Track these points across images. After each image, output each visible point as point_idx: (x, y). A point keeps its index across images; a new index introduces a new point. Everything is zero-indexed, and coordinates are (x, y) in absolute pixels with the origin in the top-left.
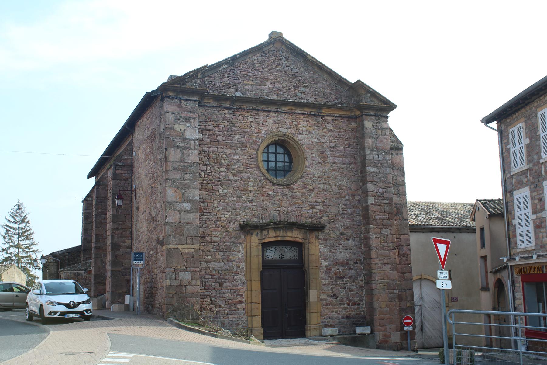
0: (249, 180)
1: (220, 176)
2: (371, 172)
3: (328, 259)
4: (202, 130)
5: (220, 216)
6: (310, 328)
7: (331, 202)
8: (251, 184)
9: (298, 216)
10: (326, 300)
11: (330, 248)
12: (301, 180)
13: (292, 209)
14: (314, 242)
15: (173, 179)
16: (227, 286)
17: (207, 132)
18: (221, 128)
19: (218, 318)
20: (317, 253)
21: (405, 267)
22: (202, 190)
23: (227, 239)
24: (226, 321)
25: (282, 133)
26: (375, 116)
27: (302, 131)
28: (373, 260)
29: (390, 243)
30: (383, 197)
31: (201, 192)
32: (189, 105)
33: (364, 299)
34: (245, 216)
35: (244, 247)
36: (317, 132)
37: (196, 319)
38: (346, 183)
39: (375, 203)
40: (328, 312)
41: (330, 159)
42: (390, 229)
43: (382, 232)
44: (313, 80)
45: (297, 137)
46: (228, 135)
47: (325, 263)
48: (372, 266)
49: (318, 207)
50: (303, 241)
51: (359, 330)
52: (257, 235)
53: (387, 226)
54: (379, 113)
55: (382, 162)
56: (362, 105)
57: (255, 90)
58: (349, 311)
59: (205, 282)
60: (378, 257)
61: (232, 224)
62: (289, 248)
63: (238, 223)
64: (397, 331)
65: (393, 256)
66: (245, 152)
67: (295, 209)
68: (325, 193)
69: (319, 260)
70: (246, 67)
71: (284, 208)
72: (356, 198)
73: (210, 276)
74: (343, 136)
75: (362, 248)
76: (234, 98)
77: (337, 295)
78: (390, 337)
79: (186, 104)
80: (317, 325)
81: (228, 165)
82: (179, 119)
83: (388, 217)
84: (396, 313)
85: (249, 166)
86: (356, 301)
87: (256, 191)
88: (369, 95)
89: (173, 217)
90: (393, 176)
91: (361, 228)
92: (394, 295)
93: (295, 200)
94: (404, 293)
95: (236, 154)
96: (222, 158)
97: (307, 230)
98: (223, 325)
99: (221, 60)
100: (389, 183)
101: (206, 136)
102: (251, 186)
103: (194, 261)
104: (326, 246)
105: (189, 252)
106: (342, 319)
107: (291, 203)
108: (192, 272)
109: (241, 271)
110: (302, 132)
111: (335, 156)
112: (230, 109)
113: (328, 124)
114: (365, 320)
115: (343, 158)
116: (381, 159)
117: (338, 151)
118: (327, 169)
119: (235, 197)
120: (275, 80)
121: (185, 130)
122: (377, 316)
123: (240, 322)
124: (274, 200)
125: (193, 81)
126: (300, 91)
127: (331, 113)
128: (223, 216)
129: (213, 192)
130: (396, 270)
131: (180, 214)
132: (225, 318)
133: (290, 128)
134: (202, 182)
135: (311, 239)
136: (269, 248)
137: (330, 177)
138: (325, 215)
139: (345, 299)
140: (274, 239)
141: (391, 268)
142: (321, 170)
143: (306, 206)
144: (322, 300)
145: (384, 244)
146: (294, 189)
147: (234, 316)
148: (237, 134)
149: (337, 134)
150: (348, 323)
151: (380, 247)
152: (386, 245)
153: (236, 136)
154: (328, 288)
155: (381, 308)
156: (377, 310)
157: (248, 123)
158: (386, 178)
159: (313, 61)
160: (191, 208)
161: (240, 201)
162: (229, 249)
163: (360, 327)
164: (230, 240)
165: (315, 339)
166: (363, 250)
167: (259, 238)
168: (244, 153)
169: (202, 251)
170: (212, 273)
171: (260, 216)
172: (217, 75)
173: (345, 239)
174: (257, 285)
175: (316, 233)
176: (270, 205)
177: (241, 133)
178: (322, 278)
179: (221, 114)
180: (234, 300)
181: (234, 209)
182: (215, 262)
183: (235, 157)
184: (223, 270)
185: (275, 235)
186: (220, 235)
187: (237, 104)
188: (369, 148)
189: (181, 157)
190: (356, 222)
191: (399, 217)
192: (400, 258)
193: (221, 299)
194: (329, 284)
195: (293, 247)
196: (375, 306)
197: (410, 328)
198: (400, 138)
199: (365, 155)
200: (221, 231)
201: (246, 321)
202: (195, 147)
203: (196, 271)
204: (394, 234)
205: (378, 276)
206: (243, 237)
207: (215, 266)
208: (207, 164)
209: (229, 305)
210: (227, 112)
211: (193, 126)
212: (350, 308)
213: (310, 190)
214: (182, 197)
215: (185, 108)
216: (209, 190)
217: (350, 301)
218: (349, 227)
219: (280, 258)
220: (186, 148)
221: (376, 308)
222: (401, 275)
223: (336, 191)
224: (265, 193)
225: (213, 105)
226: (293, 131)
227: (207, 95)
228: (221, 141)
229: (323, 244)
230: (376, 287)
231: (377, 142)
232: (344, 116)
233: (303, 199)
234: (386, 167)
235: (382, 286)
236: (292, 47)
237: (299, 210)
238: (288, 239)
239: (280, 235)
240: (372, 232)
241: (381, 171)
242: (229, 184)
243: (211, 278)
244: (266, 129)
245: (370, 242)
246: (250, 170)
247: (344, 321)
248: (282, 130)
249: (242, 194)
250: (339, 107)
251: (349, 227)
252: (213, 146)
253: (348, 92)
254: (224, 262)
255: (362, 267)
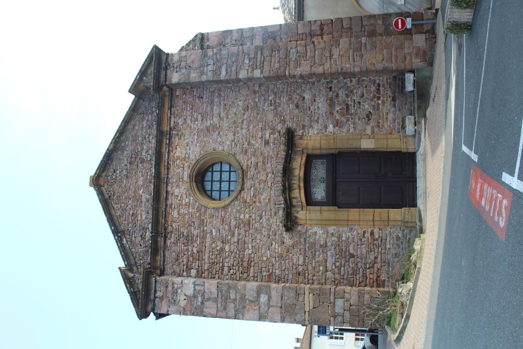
0: (237, 219)
1: (234, 252)
2: (227, 73)
3: (326, 123)
4: (187, 269)
5: (277, 254)
6: (405, 149)
7: (261, 120)
8: (242, 217)
9: (277, 161)
10: (373, 128)
11: (313, 121)
12: (238, 157)
13: (270, 168)
14: (306, 142)
15: (235, 312)
16: (354, 249)
17: (189, 263)
18: (185, 247)
19: (389, 261)
20: (318, 138)
21: (335, 27)
22: (248, 273)
23: (302, 246)
24: (393, 251)
25: (188, 179)
26: (166, 70)
27: (186, 155)
28: (326, 70)
29: (306, 49)
30: (254, 58)
31: (251, 274)
32: (160, 288)
33: (372, 78)
34: (276, 225)
35: (310, 227)
36: (187, 136)
37: (389, 295)
38: (240, 101)
39: (261, 69)
40: (387, 124)
41: (216, 120)
42: (291, 49)
43: (294, 59)
44: (134, 141)
45: (192, 160)
46: (191, 240)
47: (331, 128)
48: (333, 71)
49: (267, 136)
50: (305, 155)
51: (409, 87)
52: (298, 212)
53: (287, 53)
54: (164, 66)
55: (215, 60)
56: (154, 88)
57: (146, 207)
58: (387, 97)
59: (348, 274)
60: (323, 65)
61: (285, 240)
62: (313, 171)
63: (285, 233)
64: (411, 39)
65: (322, 45)
66: (208, 221)
67: (269, 164)
68: (251, 127)
69: (327, 135)
70: (124, 217)
71: (268, 178)
72: (257, 89)
73: (342, 268)
74: (191, 105)
75: (314, 81)
76: (153, 234)
77: (368, 113)
78: (418, 48)
79: (159, 292)
80: (402, 139)
81: (223, 242)
82: (175, 301)
83: (276, 52)
84: (390, 39)
85: (223, 217)
86: (375, 89)
87: (250, 210)
88: (144, 78)
89: (275, 315)
90: (232, 44)
91: (291, 83)
92: (368, 43)
93: (259, 164)
94: (366, 27)
95: (211, 232)
96: (216, 248)
97: (292, 151)
98: (397, 256)
99: (117, 247)
100: (239, 52)
101: (193, 265)
102: (244, 216)
103: (323, 293)
104: (311, 126)
105: (313, 299)
106: (395, 107)
107: (262, 169)
108: (336, 296)
109: (338, 232)
110: (187, 154)
111: (211, 114)
112: (166, 237)
113: (178, 123)
114: (398, 77)
115: (214, 105)
116: (212, 61)
117: (207, 111)
118: (225, 124)
119: (256, 235)
120: (136, 185)
121: (185, 295)
122: (393, 66)
123: (394, 235)
124: (259, 189)
125: (136, 282)
126: (146, 156)
127: (168, 119)
128: (276, 251)
129: (251, 260)
130: (338, 41)
131: (272, 306)
132: (389, 253)
133: (184, 169)
134: (240, 273)
135: (303, 145)
136: (312, 195)
137: (235, 121)
138: (276, 127)
139: (373, 103)
140: (302, 191)
141: (336, 47)
142: (227, 131)
143: (267, 150)
144: (373, 132)
145: (307, 57)
146: (247, 165)
147: (387, 242)
148: (191, 230)
149: (188, 112)
150: (401, 99)
151: (311, 62)
152: (309, 53)
153: (193, 231)
154: (359, 125)
155: (383, 59)
156: (386, 65)
157: (179, 217)
158: (233, 54)
159: (115, 142)
160: (265, 294)
161: (261, 230)
162: (313, 244)
163: (406, 86)
164: (303, 243)
165: (418, 145)
166: (315, 80)
167: (301, 209)
168: (210, 223)
169: (314, 276)
170: (339, 266)
171: (277, 206)
172: (133, 250)
173: (303, 103)
174: (354, 213)
175: (296, 138)
176: (265, 195)
177: (189, 226)
178: (347, 132)
179: (171, 247)
180: (370, 241)
181: (269, 238)
182: (327, 262)
183: (214, 234)
184: (336, 253)
185: (298, 190)
186: (297, 255)
187: (160, 230)
188: (200, 77)
189: (213, 301)
190: (283, 89)
191: (278, 35)
192: (325, 34)
193: (368, 257)
194: (354, 123)
195: (312, 166)
196: (381, 68)
197: (409, 21)
198: (191, 38)
199: (209, 81)
200: (292, 253)
201: (394, 227)
202: (202, 285)
203: (334, 293)
204: (297, 43)
205: (346, 64)
206: (299, 228)
207: (331, 262)
208: (222, 265)
209: (375, 248)
210: (169, 240)
211: (181, 285)
212: (383, 96)
213: (248, 146)
214: (253, 303)
215: (163, 293)
216: (249, 265)
217: (374, 97)
218: (290, 97)
219: (324, 182)
220: (203, 295)
221: (383, 68)
222: (345, 32)
223: (250, 113)
224: (252, 199)
225: (162, 255)
226: (186, 165)
227: (152, 265)
228: (198, 249)
229: (308, 130)
230: (359, 67)
231: (194, 67)
232: (170, 104)
233: (259, 154)
234: (220, 55)
235: (357, 59)
236: (102, 167)
237: (271, 159)
238: (302, 174)
239: (298, 183)
240: (294, 71)
241: (225, 62)
242: (243, 241)
243: (344, 267)
244: (185, 196)
245: (306, 75)
246: (227, 217)
247: (398, 104)
248: (186, 178)
249: (253, 227)
250: (160, 112)
251: (290, 97)
252: (204, 257)
253: (145, 100)
254: (327, 251)
255: (335, 81)
